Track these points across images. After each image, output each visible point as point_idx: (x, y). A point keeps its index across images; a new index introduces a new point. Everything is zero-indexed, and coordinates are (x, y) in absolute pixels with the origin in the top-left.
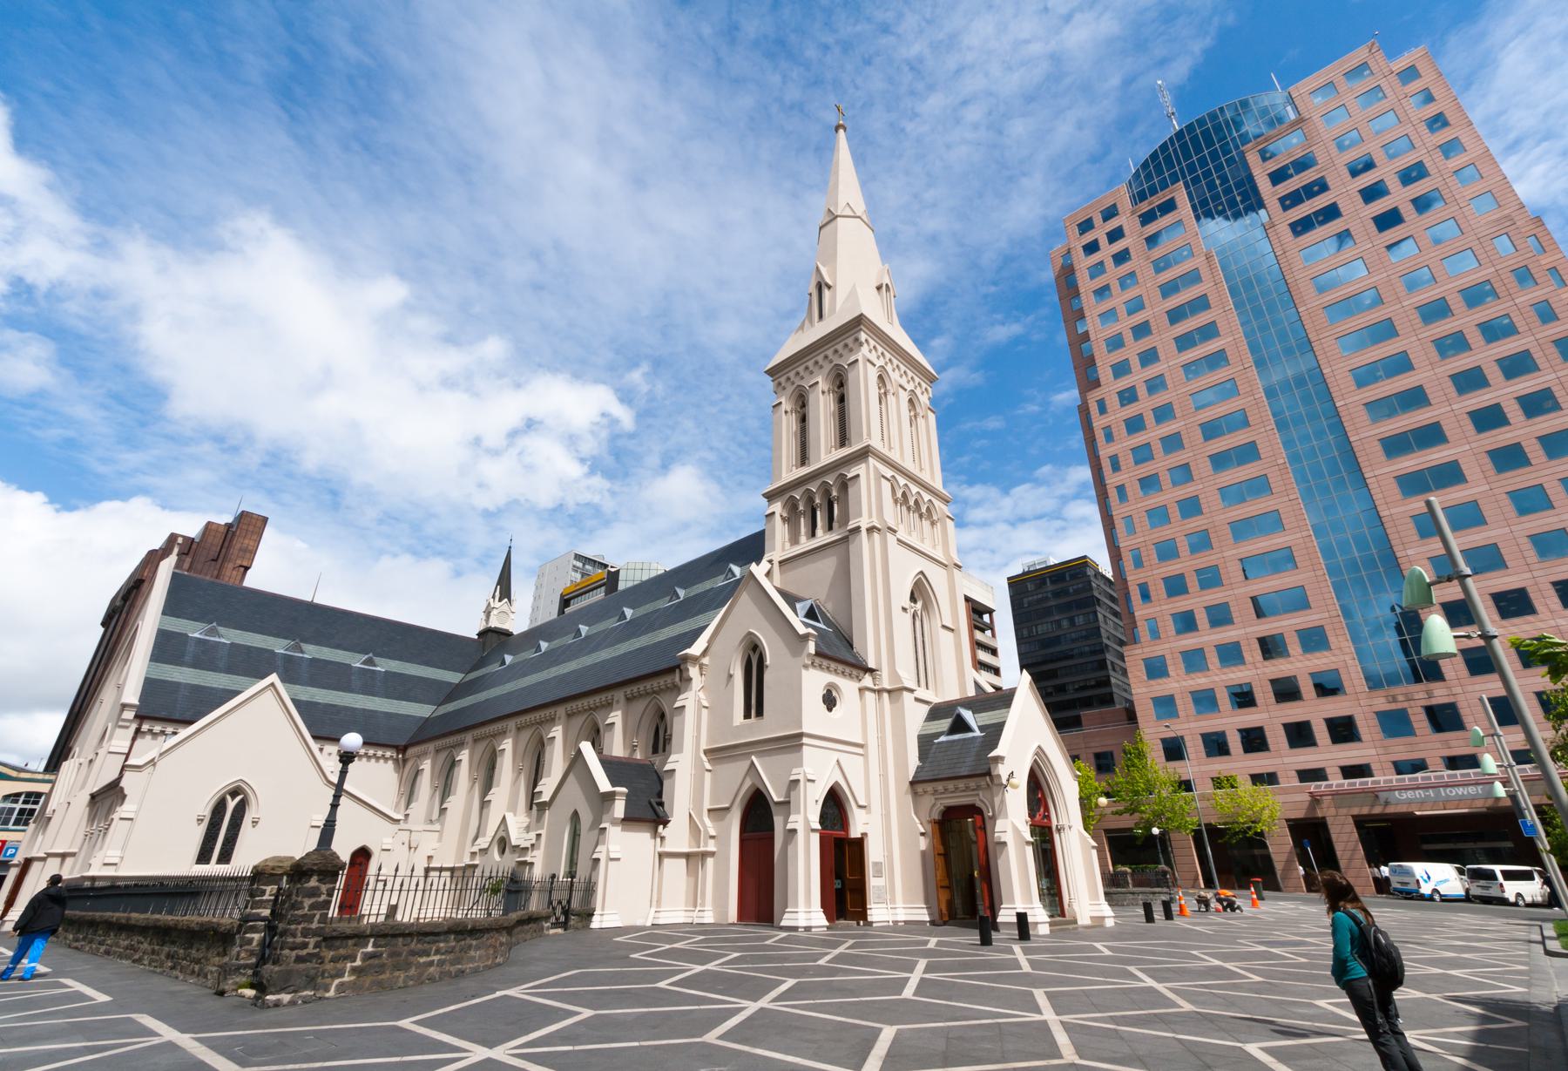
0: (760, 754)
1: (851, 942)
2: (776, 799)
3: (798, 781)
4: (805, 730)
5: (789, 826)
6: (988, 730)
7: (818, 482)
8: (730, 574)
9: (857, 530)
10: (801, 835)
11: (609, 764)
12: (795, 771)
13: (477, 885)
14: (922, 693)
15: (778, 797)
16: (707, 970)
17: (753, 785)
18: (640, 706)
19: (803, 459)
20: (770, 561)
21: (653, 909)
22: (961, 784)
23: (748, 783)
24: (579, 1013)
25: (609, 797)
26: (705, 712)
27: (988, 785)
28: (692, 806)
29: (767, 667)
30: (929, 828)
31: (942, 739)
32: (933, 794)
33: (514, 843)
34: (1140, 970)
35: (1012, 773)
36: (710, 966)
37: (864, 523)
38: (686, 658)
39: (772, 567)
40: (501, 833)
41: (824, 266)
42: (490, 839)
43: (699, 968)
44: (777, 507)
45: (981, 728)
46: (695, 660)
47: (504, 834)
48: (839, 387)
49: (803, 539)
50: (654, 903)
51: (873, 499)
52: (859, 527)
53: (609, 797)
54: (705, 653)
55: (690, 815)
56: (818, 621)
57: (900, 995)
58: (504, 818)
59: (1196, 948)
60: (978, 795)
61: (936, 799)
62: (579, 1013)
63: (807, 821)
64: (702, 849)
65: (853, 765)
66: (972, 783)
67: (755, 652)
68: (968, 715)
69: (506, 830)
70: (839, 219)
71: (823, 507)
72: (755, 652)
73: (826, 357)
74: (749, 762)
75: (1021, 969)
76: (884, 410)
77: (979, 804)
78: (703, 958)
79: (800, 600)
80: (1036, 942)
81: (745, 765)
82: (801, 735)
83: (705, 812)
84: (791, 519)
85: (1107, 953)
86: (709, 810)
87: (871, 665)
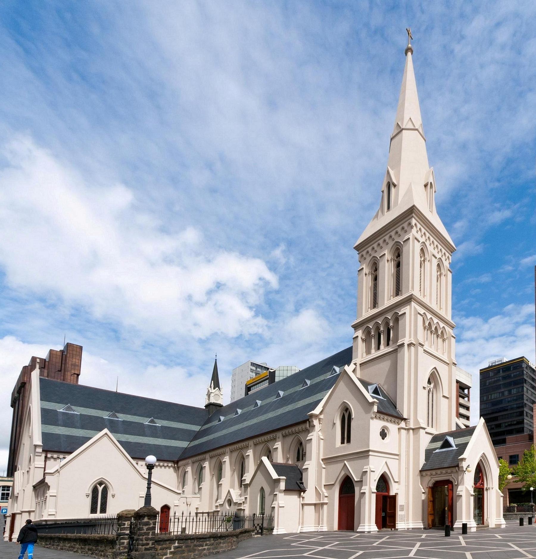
0: (348, 460)
1: (388, 537)
2: (356, 480)
4: (371, 448)
6: (460, 446)
7: (382, 318)
8: (334, 371)
9: (403, 345)
10: (367, 495)
13: (220, 519)
14: (429, 430)
19: (375, 304)
20: (355, 364)
21: (300, 526)
22: (444, 471)
25: (278, 481)
26: (322, 441)
27: (457, 471)
29: (353, 419)
30: (427, 490)
31: (437, 451)
32: (430, 476)
33: (235, 502)
34: (513, 544)
35: (469, 465)
37: (406, 342)
40: (228, 498)
44: (360, 333)
45: (456, 446)
46: (316, 416)
47: (230, 498)
48: (397, 257)
49: (373, 351)
50: (301, 524)
53: (278, 481)
54: (321, 413)
55: (316, 487)
56: (379, 395)
57: (408, 556)
59: (500, 540)
60: (452, 475)
61: (431, 478)
63: (370, 488)
64: (321, 502)
65: (393, 464)
66: (449, 470)
67: (346, 412)
68: (451, 440)
71: (384, 332)
72: (346, 412)
75: (462, 545)
77: (451, 479)
79: (371, 384)
80: (469, 534)
81: (342, 465)
82: (369, 451)
83: (323, 486)
84: (367, 340)
85: (500, 538)
87: (405, 416)
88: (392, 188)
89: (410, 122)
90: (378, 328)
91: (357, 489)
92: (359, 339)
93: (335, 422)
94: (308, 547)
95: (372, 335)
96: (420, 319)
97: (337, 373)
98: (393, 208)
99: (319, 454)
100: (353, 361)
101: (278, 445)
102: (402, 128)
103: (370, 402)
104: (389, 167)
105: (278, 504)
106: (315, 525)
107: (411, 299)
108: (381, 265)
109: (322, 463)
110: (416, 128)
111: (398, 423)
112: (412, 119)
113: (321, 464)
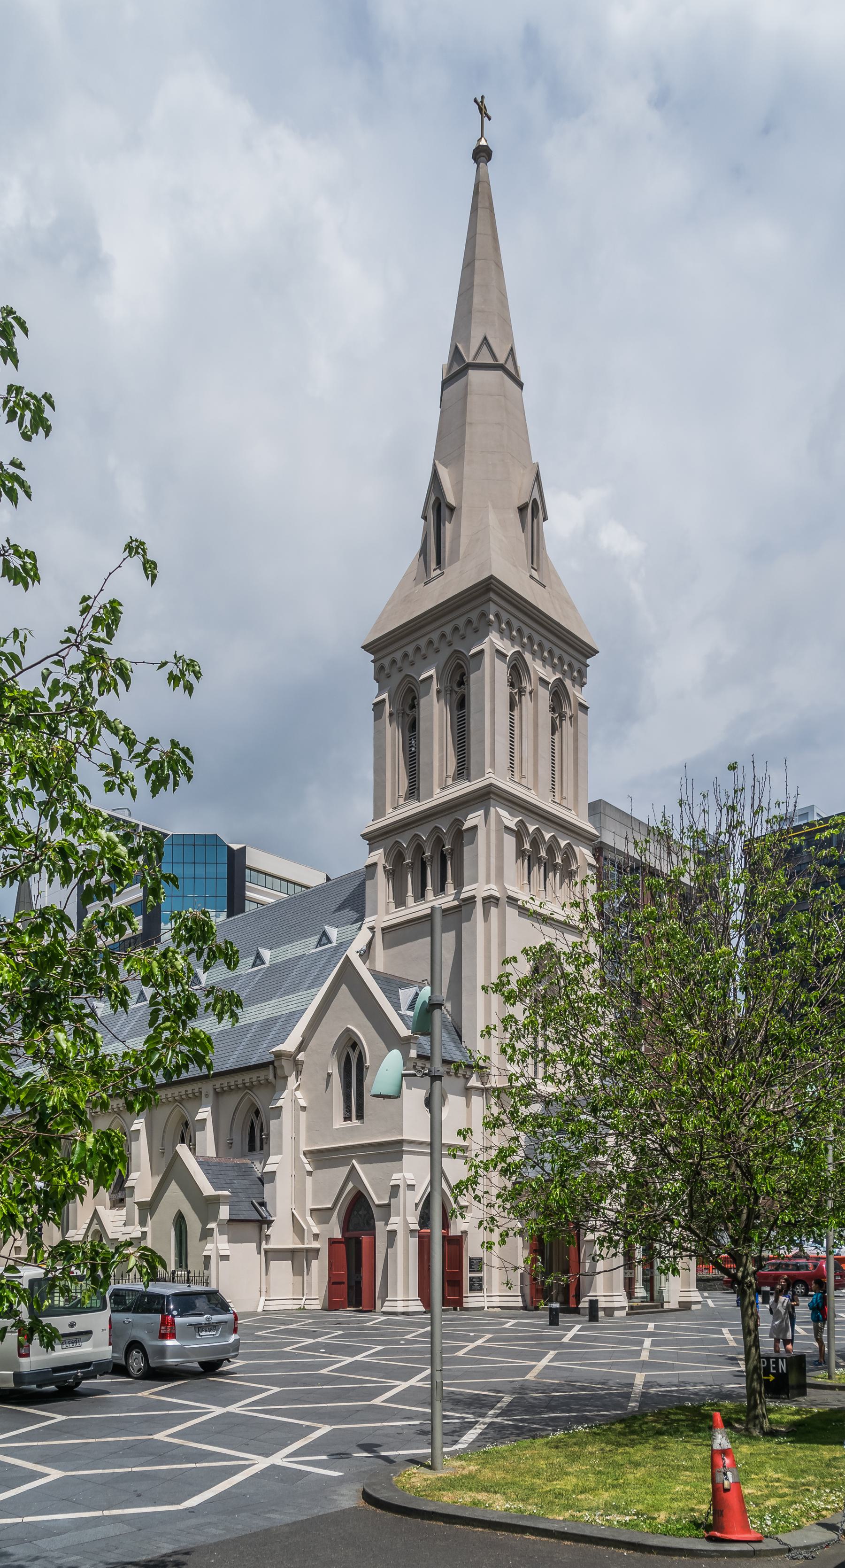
0: (363, 1160)
2: (377, 1202)
3: (398, 1186)
4: (405, 1137)
5: (389, 1227)
7: (429, 827)
8: (324, 938)
9: (471, 900)
11: (205, 1164)
12: (395, 1176)
15: (379, 1198)
16: (411, 1386)
17: (354, 1187)
18: (231, 1102)
19: (413, 792)
20: (372, 929)
21: (263, 1299)
23: (350, 1186)
24: (168, 1436)
26: (303, 1115)
28: (294, 1206)
29: (367, 1068)
33: (111, 1236)
36: (359, 1358)
37: (481, 894)
38: (279, 1055)
39: (373, 937)
40: (95, 1226)
41: (445, 465)
42: (84, 1232)
43: (349, 1360)
44: (378, 856)
46: (292, 1057)
47: (98, 1227)
49: (410, 900)
50: (263, 1293)
51: (493, 860)
52: (474, 897)
53: (214, 1202)
54: (301, 1047)
55: (293, 1214)
58: (96, 1210)
62: (168, 1436)
63: (406, 1223)
64: (306, 1246)
69: (100, 1223)
70: (472, 373)
73: (443, 636)
74: (347, 1169)
76: (516, 718)
78: (314, 1335)
81: (345, 1170)
82: (401, 1142)
83: (308, 1213)
84: (395, 874)
86: (312, 1210)
88: (444, 525)
89: (485, 348)
90: (419, 849)
91: (379, 1225)
92: (380, 871)
93: (330, 1071)
94: (386, 1360)
95: (408, 864)
96: (510, 842)
97: (331, 943)
98: (450, 564)
99: (296, 1139)
100: (367, 920)
101: (205, 1113)
102: (467, 361)
103: (402, 1035)
104: (437, 462)
105: (217, 1249)
106: (294, 1294)
107: (489, 793)
108: (423, 701)
109: (305, 1160)
110: (501, 361)
111: (464, 1076)
112: (491, 341)
113: (303, 1163)
